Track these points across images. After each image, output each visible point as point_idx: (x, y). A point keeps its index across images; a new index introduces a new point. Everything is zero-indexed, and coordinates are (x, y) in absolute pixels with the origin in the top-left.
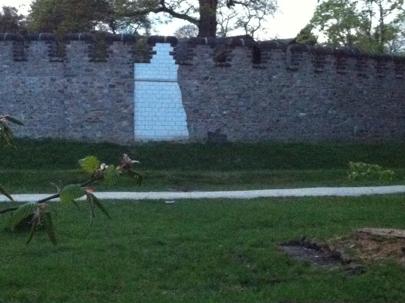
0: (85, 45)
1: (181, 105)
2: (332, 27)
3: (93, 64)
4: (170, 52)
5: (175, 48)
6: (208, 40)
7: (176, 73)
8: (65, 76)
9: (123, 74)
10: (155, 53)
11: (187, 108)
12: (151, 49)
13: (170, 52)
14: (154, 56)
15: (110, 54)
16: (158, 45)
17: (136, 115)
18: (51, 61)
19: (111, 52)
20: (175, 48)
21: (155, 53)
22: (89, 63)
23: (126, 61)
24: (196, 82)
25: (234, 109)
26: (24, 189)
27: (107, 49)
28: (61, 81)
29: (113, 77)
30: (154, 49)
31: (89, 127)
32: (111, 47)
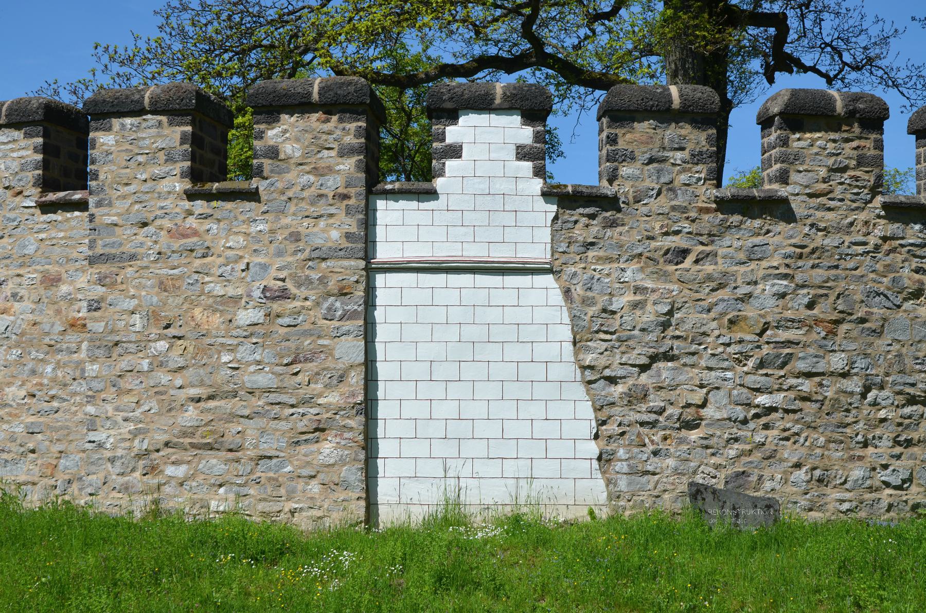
0: (167, 131)
1: (570, 371)
2: (784, 221)
3: (200, 206)
4: (519, 147)
5: (540, 128)
6: (681, 96)
7: (545, 235)
8: (93, 261)
9: (318, 242)
10: (455, 152)
11: (594, 377)
12: (442, 137)
13: (519, 147)
14: (451, 165)
15: (267, 163)
16: (468, 120)
17: (404, 517)
18: (46, 208)
19: (273, 153)
20: (540, 128)
21: (455, 152)
22: (187, 204)
23: (334, 183)
24: (632, 273)
25: (807, 386)
26: (802, 94)
27: (257, 144)
28: (82, 283)
29: (280, 253)
30: (453, 133)
31: (180, 471)
32: (270, 133)
